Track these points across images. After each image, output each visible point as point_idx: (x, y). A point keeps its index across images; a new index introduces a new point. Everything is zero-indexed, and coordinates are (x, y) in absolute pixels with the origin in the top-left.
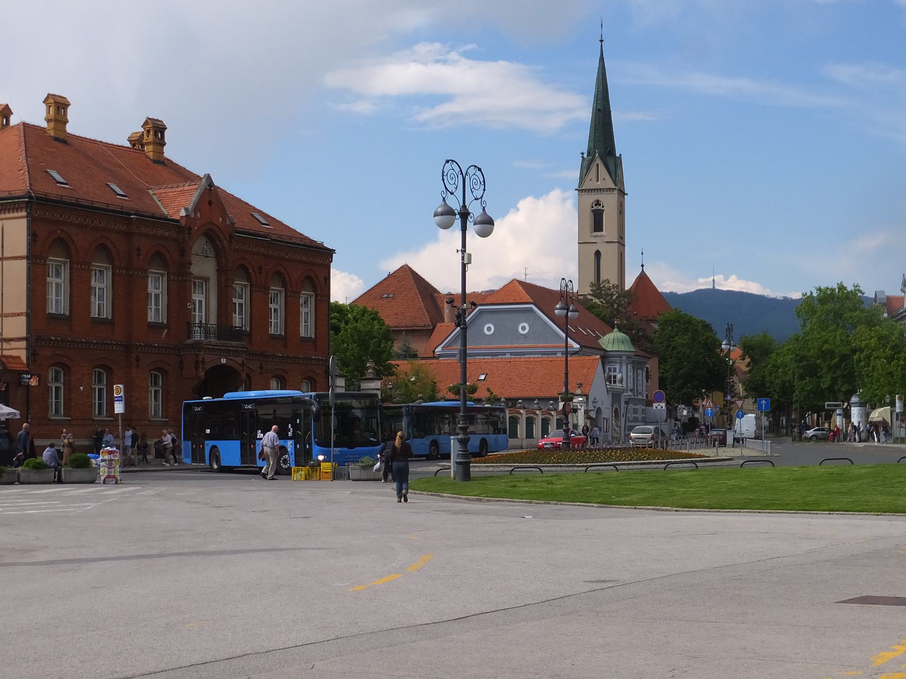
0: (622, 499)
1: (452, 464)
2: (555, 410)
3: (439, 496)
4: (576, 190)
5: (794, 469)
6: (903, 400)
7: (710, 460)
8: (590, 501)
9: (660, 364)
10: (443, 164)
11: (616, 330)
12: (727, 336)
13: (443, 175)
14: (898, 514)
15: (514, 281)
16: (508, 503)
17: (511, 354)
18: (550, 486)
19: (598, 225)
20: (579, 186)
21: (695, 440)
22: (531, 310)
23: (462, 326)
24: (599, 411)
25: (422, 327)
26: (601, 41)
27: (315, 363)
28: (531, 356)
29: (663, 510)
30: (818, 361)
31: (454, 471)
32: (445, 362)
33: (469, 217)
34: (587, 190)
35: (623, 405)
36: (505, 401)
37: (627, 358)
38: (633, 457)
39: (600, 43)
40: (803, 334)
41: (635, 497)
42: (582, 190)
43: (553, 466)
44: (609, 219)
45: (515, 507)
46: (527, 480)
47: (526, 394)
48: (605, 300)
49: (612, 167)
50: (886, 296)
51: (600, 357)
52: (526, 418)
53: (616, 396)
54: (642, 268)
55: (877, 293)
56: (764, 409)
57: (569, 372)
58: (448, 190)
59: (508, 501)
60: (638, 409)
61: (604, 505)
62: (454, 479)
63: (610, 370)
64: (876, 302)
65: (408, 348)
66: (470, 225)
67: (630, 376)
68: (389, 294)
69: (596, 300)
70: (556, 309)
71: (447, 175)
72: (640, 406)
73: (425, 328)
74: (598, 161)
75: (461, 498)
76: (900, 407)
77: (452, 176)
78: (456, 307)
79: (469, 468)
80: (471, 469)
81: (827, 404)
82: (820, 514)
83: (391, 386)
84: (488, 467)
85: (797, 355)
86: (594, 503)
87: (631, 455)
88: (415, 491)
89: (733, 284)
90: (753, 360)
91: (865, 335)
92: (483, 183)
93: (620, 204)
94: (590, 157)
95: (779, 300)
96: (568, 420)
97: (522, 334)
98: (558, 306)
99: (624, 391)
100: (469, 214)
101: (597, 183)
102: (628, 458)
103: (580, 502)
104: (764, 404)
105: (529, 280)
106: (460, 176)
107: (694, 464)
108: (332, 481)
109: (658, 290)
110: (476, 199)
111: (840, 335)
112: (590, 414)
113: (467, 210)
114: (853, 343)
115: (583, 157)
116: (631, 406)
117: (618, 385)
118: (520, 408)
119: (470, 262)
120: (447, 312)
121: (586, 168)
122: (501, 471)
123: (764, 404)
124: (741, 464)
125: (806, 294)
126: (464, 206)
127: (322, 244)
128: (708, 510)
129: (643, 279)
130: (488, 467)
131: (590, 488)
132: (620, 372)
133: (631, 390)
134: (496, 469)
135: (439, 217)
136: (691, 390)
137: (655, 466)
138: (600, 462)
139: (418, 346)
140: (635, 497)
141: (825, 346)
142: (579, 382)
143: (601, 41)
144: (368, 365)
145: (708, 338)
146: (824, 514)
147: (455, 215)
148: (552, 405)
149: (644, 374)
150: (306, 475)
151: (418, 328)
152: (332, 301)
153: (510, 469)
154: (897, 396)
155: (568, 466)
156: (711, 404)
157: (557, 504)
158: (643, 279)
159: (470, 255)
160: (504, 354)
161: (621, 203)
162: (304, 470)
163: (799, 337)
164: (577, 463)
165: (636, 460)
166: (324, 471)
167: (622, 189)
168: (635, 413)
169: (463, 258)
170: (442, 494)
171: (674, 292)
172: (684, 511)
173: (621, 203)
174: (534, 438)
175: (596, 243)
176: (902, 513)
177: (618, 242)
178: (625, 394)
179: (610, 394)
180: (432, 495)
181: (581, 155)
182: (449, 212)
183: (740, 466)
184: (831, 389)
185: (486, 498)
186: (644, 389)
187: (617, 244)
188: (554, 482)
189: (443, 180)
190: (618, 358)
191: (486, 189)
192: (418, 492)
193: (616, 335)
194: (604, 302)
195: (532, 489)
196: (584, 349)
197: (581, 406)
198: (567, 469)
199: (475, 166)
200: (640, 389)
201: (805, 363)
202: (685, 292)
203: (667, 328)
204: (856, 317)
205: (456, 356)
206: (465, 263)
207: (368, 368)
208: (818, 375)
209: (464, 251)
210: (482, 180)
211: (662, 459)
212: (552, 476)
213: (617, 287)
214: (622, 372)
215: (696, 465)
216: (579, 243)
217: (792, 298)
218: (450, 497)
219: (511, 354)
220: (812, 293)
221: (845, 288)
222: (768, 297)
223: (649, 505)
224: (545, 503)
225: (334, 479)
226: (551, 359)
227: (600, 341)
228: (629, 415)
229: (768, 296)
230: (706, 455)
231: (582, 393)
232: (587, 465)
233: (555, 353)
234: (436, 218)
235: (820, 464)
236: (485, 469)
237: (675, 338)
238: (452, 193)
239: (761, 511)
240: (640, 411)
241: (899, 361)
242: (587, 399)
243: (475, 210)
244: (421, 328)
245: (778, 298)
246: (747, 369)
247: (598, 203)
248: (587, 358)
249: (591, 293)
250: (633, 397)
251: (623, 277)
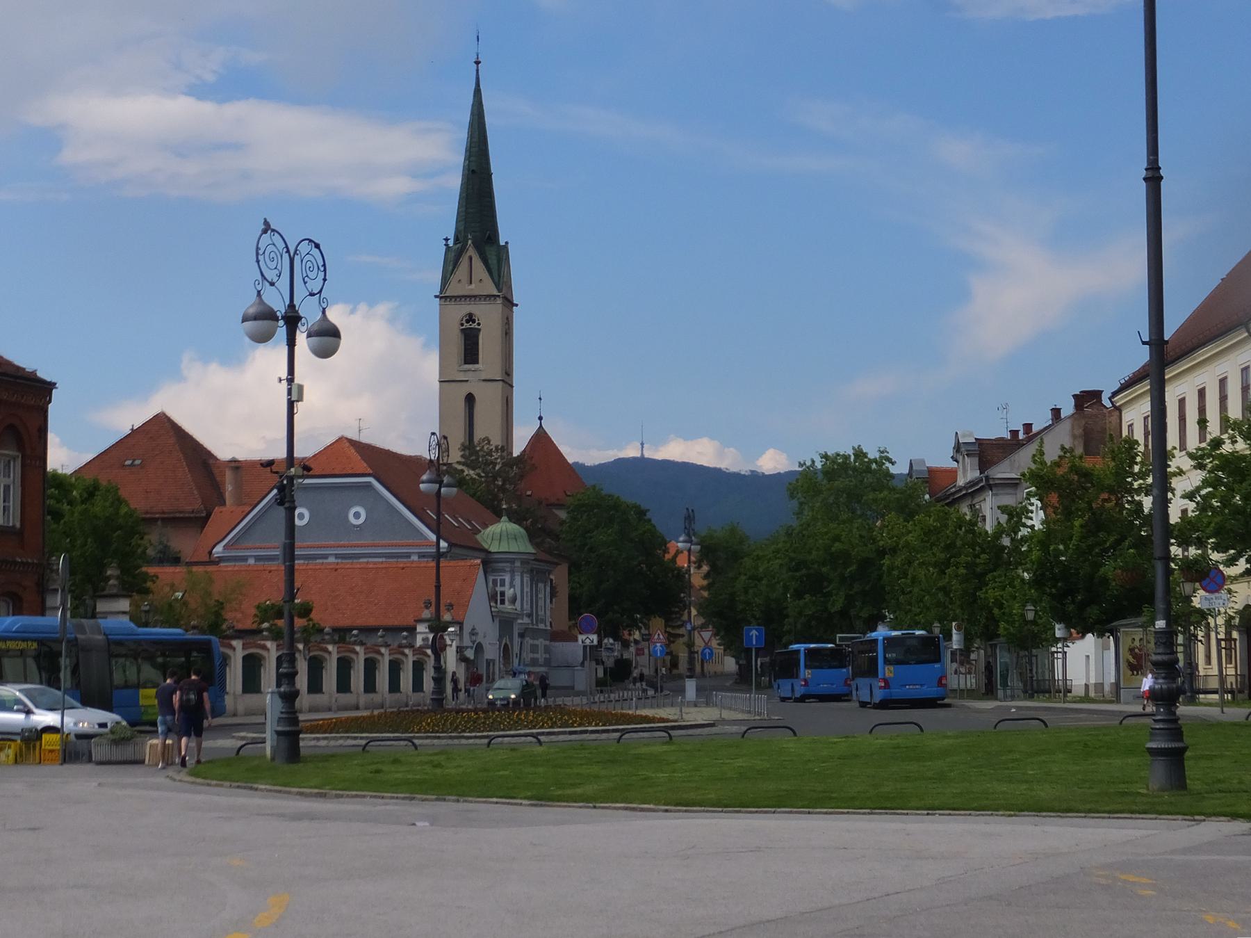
0: (569, 792)
1: (269, 735)
2: (411, 646)
3: (251, 788)
4: (436, 297)
5: (830, 740)
6: (963, 630)
7: (680, 726)
8: (515, 795)
9: (570, 573)
10: (258, 236)
11: (504, 518)
12: (685, 528)
13: (257, 254)
14: (1044, 814)
15: (341, 440)
16: (372, 799)
17: (337, 556)
18: (438, 771)
19: (471, 354)
20: (441, 292)
21: (621, 695)
22: (368, 486)
23: (287, 505)
24: (479, 649)
25: (189, 513)
26: (477, 63)
27: (21, 569)
28: (370, 560)
29: (642, 810)
30: (824, 569)
31: (272, 747)
32: (229, 569)
33: (299, 324)
34: (453, 297)
35: (516, 640)
36: (331, 631)
37: (521, 564)
38: (555, 722)
39: (476, 65)
40: (800, 526)
41: (589, 789)
42: (446, 297)
43: (427, 738)
44: (488, 345)
45: (388, 807)
46: (396, 761)
47: (360, 622)
48: (483, 472)
49: (493, 261)
50: (927, 467)
51: (482, 562)
52: (338, 659)
53: (505, 624)
54: (539, 421)
55: (913, 462)
56: (754, 643)
57: (442, 583)
58: (265, 279)
59: (371, 797)
60: (538, 646)
61: (540, 803)
62: (273, 759)
63: (495, 582)
64: (911, 477)
65: (166, 546)
66: (301, 338)
67: (527, 592)
68: (134, 460)
69: (469, 472)
70: (423, 482)
71: (264, 253)
72: (541, 640)
73: (192, 515)
74: (471, 252)
75: (289, 793)
76: (958, 641)
77: (273, 255)
78: (277, 473)
79: (297, 741)
80: (301, 744)
81: (840, 637)
82: (912, 814)
83: (147, 608)
84: (318, 739)
85: (792, 559)
86: (521, 798)
87: (551, 719)
88: (209, 781)
89: (674, 451)
90: (714, 568)
91: (899, 528)
92: (322, 269)
93: (506, 321)
94: (458, 245)
95: (744, 475)
96: (294, 667)
97: (354, 526)
98: (424, 477)
99: (520, 616)
100: (300, 318)
101: (470, 287)
102: (548, 724)
103: (497, 797)
104: (754, 637)
105: (365, 438)
106: (286, 256)
107: (665, 732)
108: (62, 764)
109: (565, 460)
110: (312, 294)
111: (858, 528)
112: (465, 653)
113: (297, 312)
114: (880, 540)
115: (446, 245)
116: (529, 641)
117: (508, 607)
118: (355, 643)
119: (300, 399)
120: (230, 489)
121: (452, 263)
122: (341, 746)
123: (754, 637)
124: (743, 732)
125: (805, 464)
126: (292, 306)
127: (34, 373)
128: (720, 809)
129: (541, 439)
130: (318, 739)
131: (506, 773)
132: (512, 586)
133: (530, 615)
134: (332, 743)
135: (250, 322)
136: (619, 615)
137: (594, 736)
138: (503, 730)
139: (183, 543)
140: (589, 789)
141: (836, 545)
142: (448, 601)
143: (477, 63)
144: (109, 572)
145: (645, 532)
146: (919, 814)
147: (277, 319)
148: (405, 638)
149: (548, 589)
150: (16, 755)
151: (181, 515)
152: (50, 467)
153: (364, 742)
154: (954, 624)
155: (451, 738)
156: (661, 637)
157: (458, 801)
158: (541, 439)
159: (301, 388)
160: (325, 557)
161: (507, 318)
162: (13, 746)
163: (793, 530)
164: (464, 731)
165: (560, 727)
166: (47, 747)
167: (509, 298)
168: (533, 653)
169: (290, 392)
170: (255, 786)
171: (580, 462)
172: (679, 811)
173: (507, 318)
174: (323, 693)
175: (467, 381)
176: (1050, 811)
177: (503, 381)
178: (520, 621)
179: (497, 621)
180: (238, 787)
181: (444, 242)
182: (268, 315)
183: (740, 735)
184: (844, 613)
185: (334, 792)
186: (548, 613)
187: (501, 383)
188: (443, 763)
189: (258, 261)
190: (508, 564)
191: (327, 278)
192: (214, 782)
193: (504, 528)
194: (483, 475)
195: (409, 777)
196: (456, 550)
197: (452, 641)
198: (450, 742)
199: (311, 241)
200: (541, 613)
201: (804, 571)
202: (597, 463)
203: (581, 517)
204: (882, 499)
205: (278, 559)
206: (293, 399)
207: (109, 578)
208: (824, 591)
209: (290, 380)
210: (321, 263)
211: (603, 725)
212: (436, 754)
213: (503, 449)
214: (514, 586)
215: (669, 734)
216: (440, 382)
217: (763, 473)
218: (270, 791)
219: (337, 556)
220: (813, 462)
221: (865, 455)
222: (727, 471)
223: (617, 802)
224: (437, 800)
225: (64, 761)
226: (401, 565)
227: (478, 537)
228: (524, 655)
229: (727, 469)
230: (671, 717)
231: (453, 619)
232: (491, 736)
233: (408, 556)
234: (247, 324)
235: (871, 732)
236: (313, 743)
237: (594, 533)
238: (272, 284)
239: (811, 810)
240: (541, 649)
241: (958, 568)
242: (461, 629)
243: (309, 312)
244: (187, 515)
245: (743, 473)
246: (705, 583)
247: (470, 318)
248: (462, 563)
249: (463, 460)
250: (531, 626)
251: (509, 438)
